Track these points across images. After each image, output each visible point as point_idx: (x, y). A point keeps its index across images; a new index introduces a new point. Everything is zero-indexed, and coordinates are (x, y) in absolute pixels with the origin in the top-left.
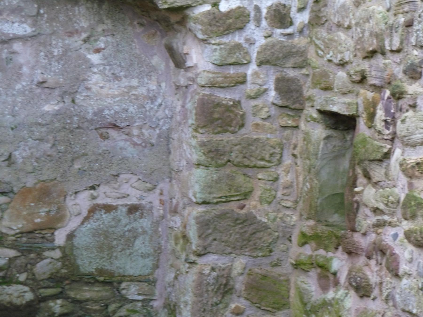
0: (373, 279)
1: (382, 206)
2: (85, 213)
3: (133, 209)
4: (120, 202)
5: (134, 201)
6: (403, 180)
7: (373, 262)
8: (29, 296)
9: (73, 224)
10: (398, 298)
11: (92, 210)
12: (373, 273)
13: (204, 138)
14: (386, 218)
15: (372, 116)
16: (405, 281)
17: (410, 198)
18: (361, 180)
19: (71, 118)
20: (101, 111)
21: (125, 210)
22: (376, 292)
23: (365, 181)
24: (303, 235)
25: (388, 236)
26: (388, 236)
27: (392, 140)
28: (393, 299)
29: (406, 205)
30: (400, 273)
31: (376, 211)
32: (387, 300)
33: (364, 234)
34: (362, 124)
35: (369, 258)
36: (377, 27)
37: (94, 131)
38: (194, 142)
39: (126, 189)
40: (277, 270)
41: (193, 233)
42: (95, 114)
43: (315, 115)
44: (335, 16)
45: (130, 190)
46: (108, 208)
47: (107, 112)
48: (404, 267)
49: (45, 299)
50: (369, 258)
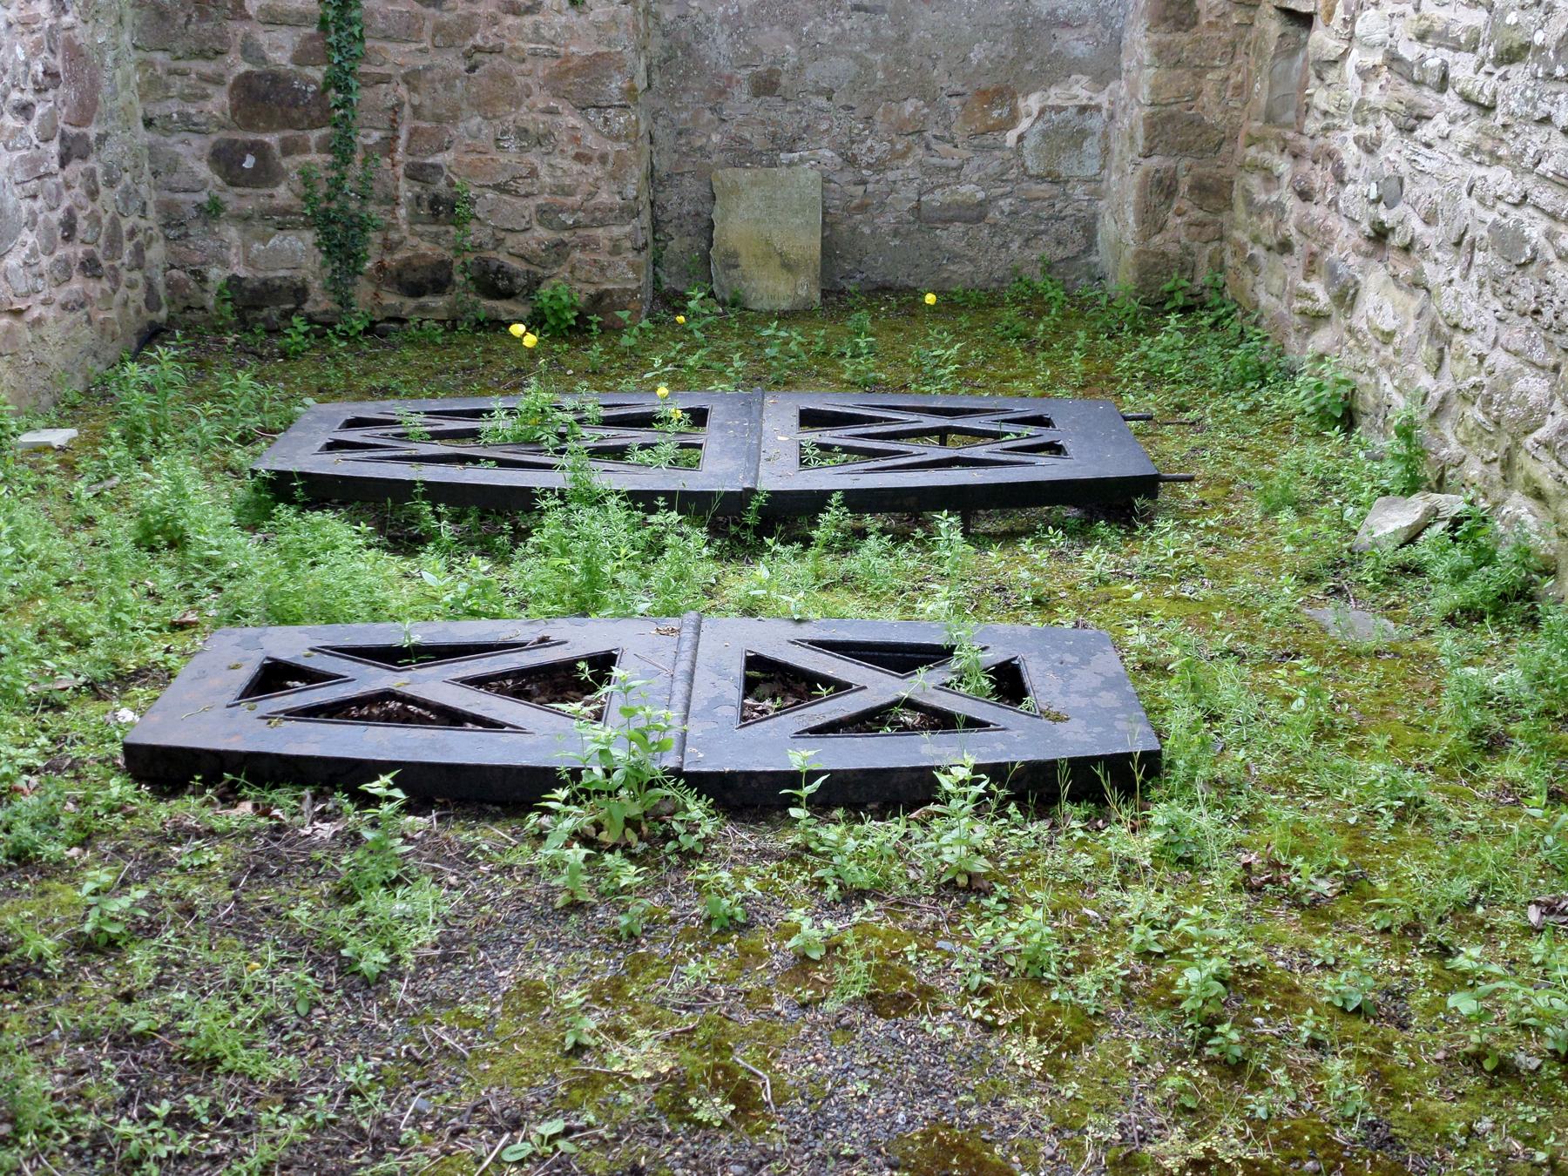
0: (1318, 185)
1: (1333, 110)
2: (1035, 114)
3: (1083, 109)
4: (1070, 103)
5: (1085, 102)
6: (1359, 82)
7: (1318, 167)
8: (981, 195)
9: (1024, 124)
10: (1341, 204)
11: (1042, 112)
12: (1320, 177)
13: (1155, 37)
14: (1336, 121)
15: (1330, 14)
16: (1350, 187)
17: (1362, 102)
18: (1314, 81)
19: (1025, 18)
20: (1055, 10)
21: (1075, 110)
22: (1318, 197)
23: (1317, 82)
24: (1249, 135)
25: (1334, 141)
26: (1334, 141)
27: (1350, 40)
28: (1336, 204)
29: (1358, 109)
30: (1346, 178)
31: (1325, 113)
32: (1329, 205)
33: (1312, 138)
34: (1318, 21)
35: (1315, 162)
36: (1446, 303)
37: (616, 512)
38: (1144, 41)
39: (1076, 90)
40: (1222, 171)
41: (1140, 134)
42: (1049, 14)
43: (1272, 11)
44: (1291, 1106)
45: (1080, 90)
46: (1059, 109)
47: (1060, 11)
48: (1350, 172)
49: (996, 199)
50: (1315, 162)
